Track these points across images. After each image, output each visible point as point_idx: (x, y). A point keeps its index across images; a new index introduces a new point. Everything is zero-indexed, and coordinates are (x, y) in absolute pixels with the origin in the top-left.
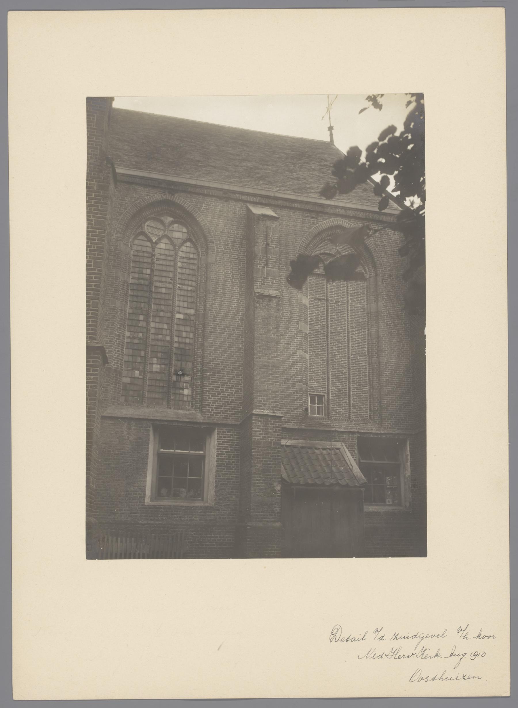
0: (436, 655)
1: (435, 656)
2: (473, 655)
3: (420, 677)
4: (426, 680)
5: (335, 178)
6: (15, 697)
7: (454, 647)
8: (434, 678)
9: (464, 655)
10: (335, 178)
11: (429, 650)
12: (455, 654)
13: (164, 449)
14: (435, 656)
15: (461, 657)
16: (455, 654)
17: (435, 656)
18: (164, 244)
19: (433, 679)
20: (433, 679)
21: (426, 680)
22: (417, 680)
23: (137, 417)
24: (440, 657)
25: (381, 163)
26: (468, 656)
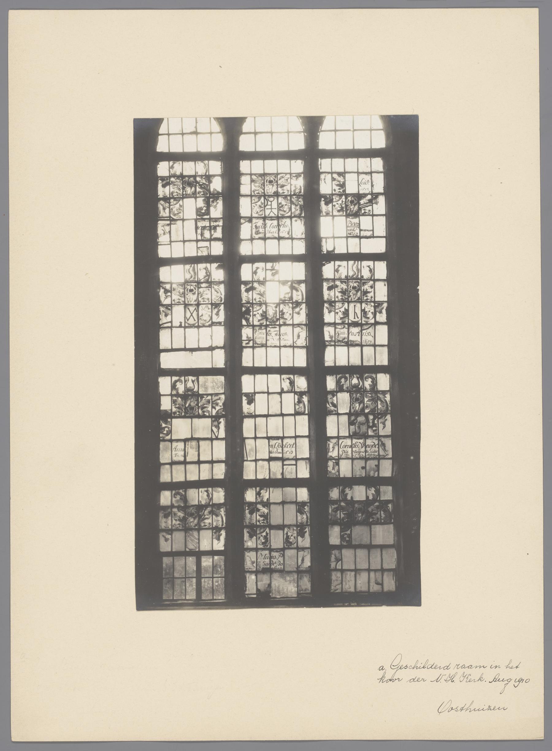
0: (480, 679)
1: (478, 680)
2: (517, 680)
3: (450, 707)
4: (456, 710)
5: (228, 366)
6: (15, 737)
7: (498, 675)
8: (463, 708)
9: (509, 680)
10: (228, 366)
11: (489, 682)
12: (499, 679)
13: (365, 603)
14: (478, 680)
15: (506, 682)
16: (499, 679)
17: (479, 680)
18: (170, 408)
19: (462, 710)
20: (462, 710)
21: (456, 710)
22: (447, 710)
23: (187, 495)
24: (484, 681)
25: (392, 520)
26: (512, 682)
